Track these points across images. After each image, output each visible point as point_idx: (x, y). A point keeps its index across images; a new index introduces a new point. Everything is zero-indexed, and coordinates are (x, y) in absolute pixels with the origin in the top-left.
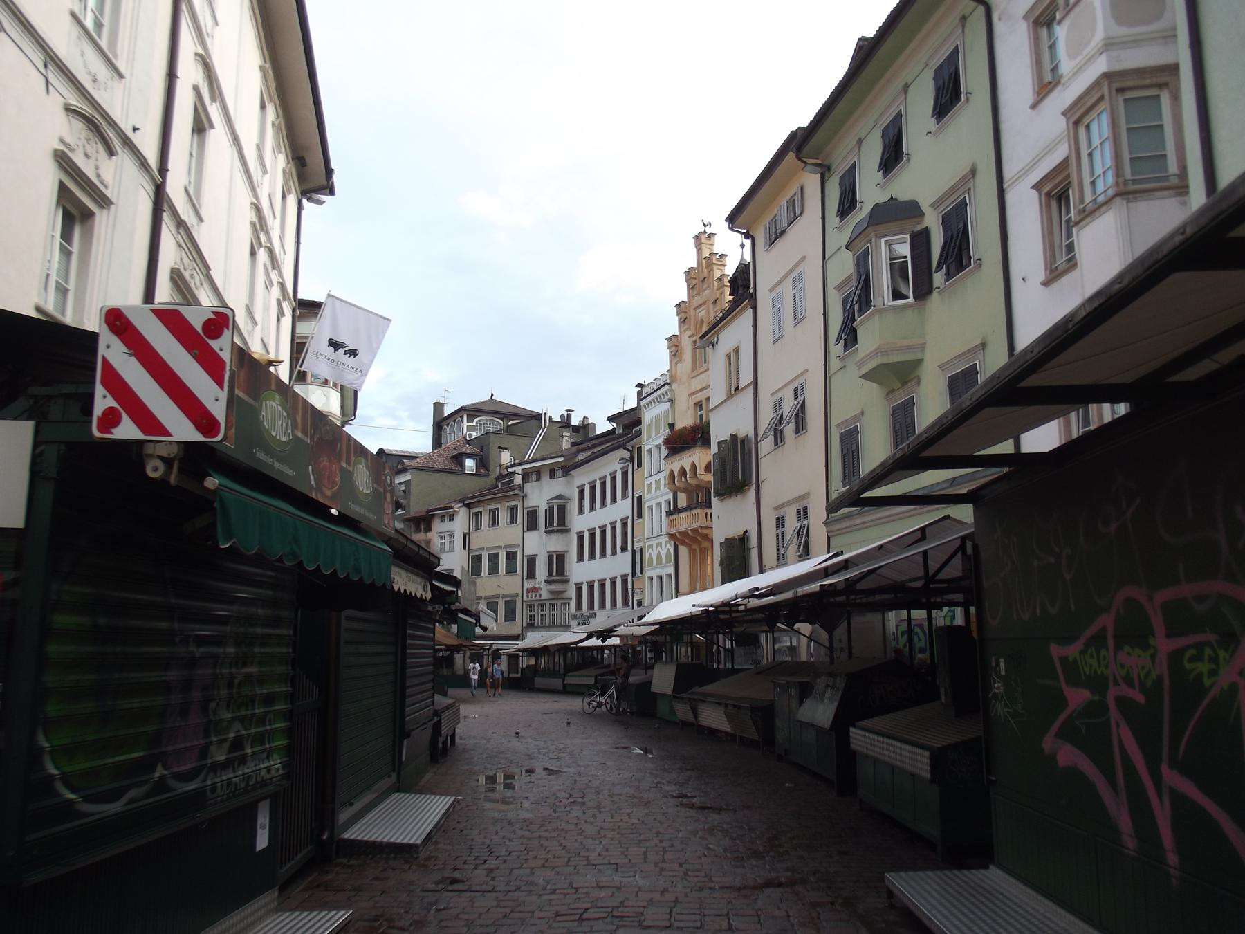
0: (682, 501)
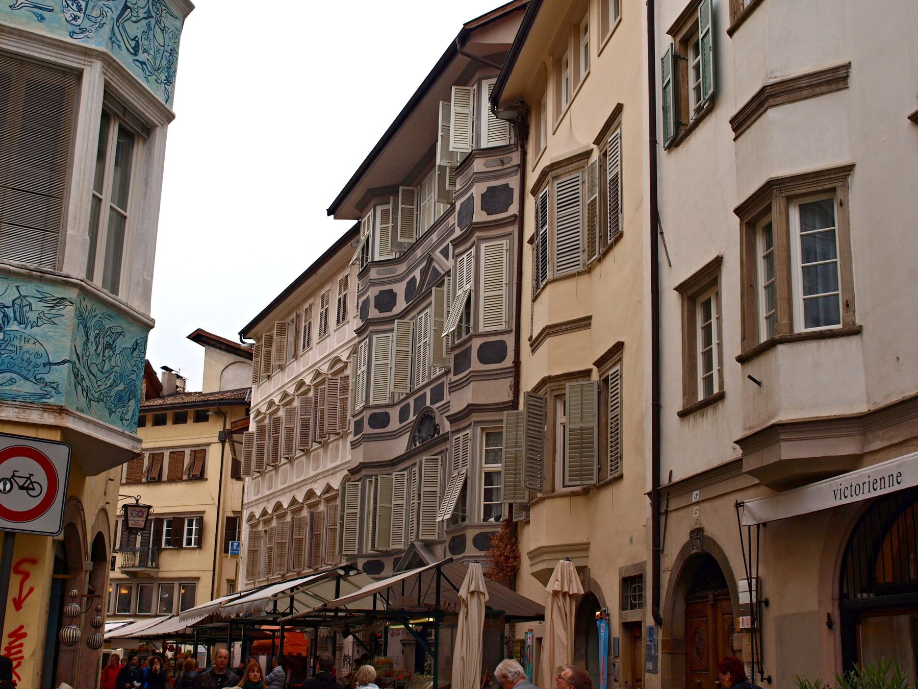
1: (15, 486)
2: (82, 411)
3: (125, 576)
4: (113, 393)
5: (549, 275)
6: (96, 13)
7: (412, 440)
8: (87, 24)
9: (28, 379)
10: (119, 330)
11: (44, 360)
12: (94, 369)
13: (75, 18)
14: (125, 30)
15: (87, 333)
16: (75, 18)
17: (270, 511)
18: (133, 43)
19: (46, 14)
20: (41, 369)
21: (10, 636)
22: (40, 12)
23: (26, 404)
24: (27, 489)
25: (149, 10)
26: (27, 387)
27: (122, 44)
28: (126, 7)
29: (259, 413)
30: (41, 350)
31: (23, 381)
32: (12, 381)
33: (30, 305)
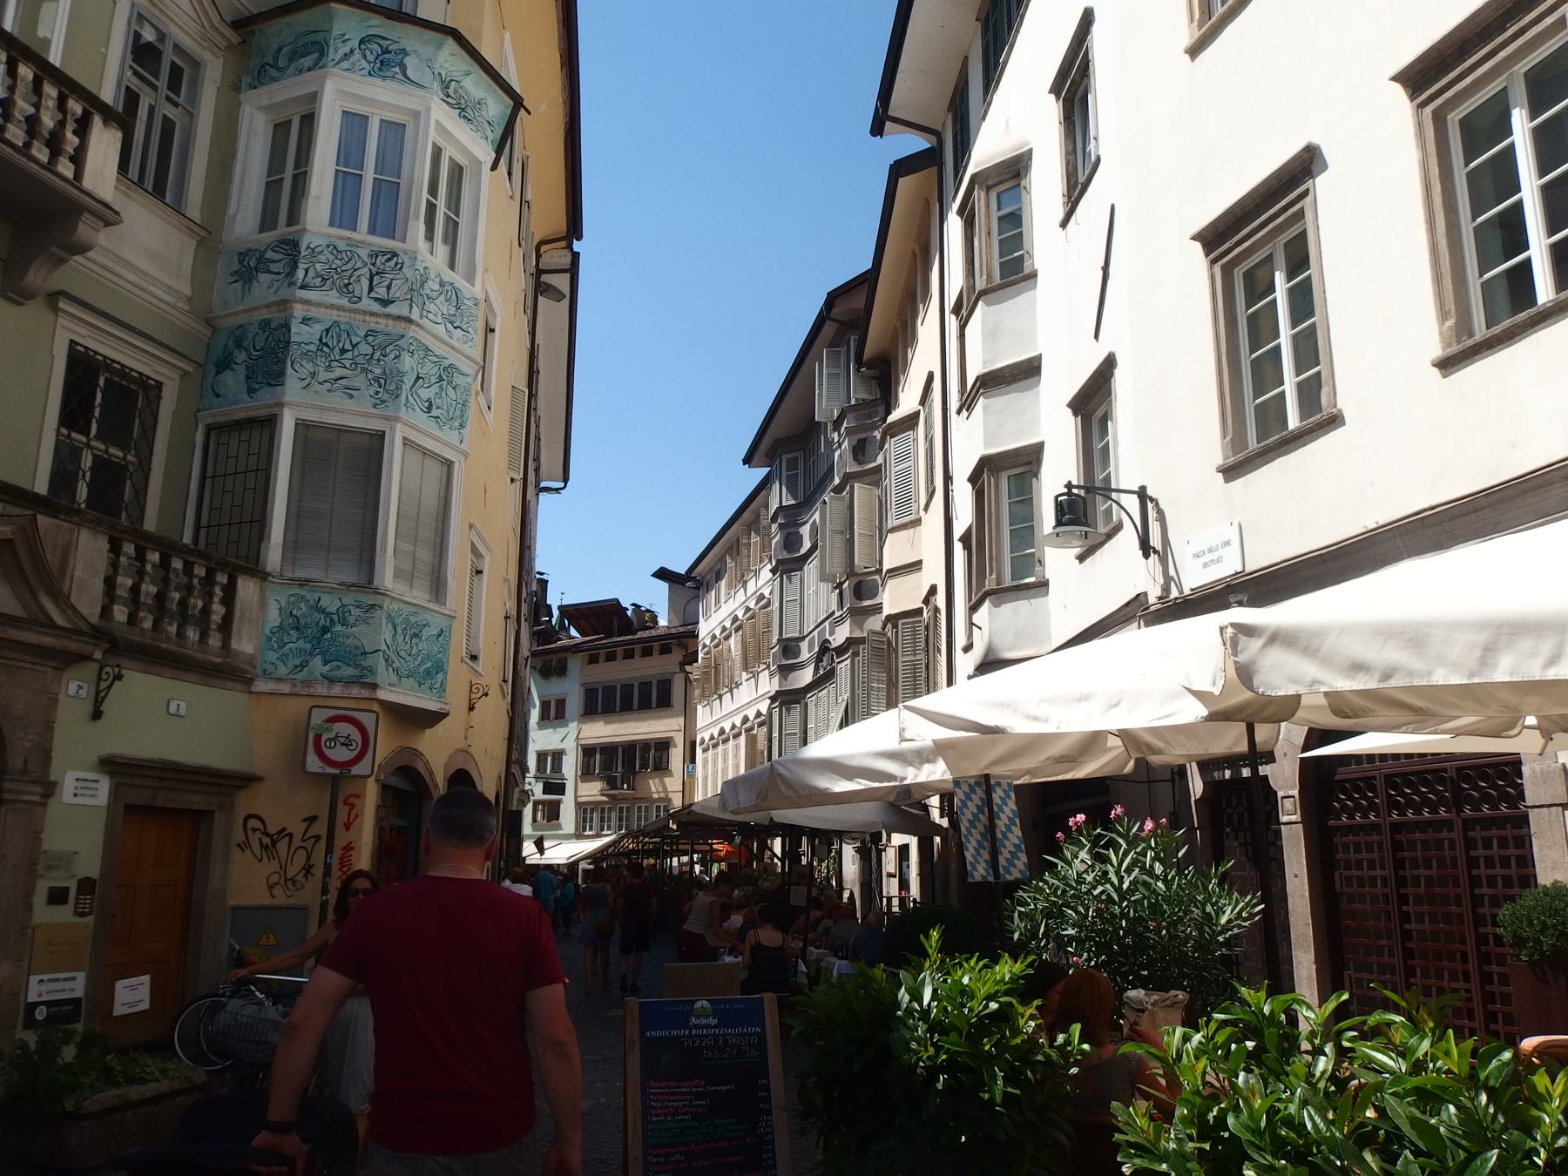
1: (338, 744)
2: (393, 685)
3: (605, 799)
4: (422, 669)
5: (891, 523)
6: (393, 387)
7: (816, 669)
8: (386, 396)
9: (349, 665)
10: (424, 622)
11: (361, 651)
12: (403, 654)
13: (377, 393)
14: (419, 396)
15: (395, 629)
16: (377, 393)
17: (716, 736)
18: (427, 404)
19: (353, 392)
20: (359, 657)
21: (343, 849)
22: (350, 391)
23: (349, 682)
24: (347, 745)
25: (440, 375)
26: (349, 671)
27: (416, 407)
28: (418, 378)
29: (705, 646)
30: (359, 644)
31: (346, 667)
32: (338, 668)
33: (350, 611)
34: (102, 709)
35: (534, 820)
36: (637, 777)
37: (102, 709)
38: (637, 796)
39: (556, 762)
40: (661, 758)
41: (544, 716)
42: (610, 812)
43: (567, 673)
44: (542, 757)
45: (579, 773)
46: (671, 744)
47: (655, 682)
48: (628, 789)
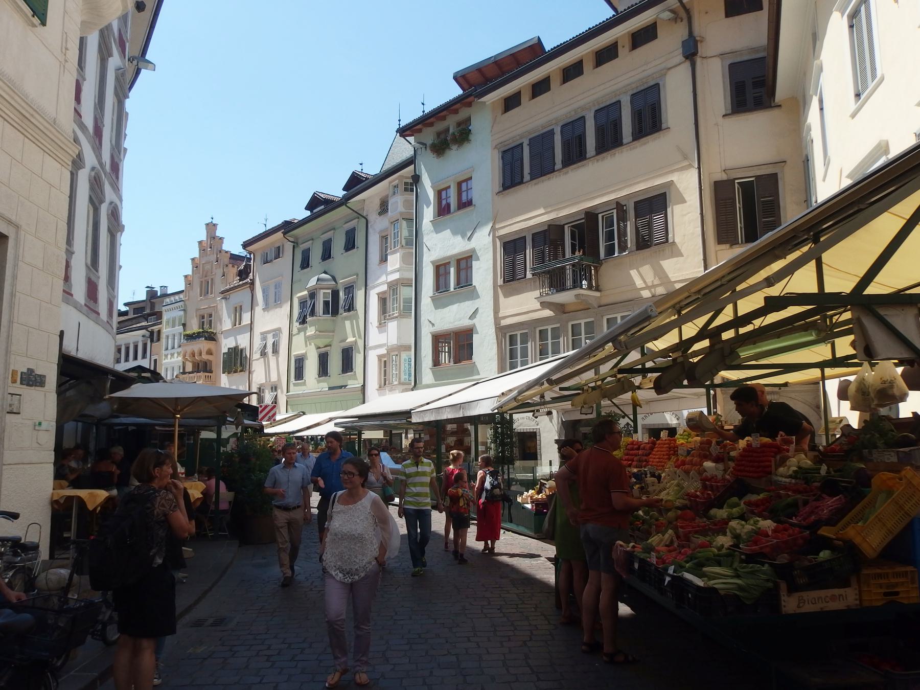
0: (189, 368)
3: (548, 313)
34: (456, 91)
35: (436, 362)
36: (604, 269)
37: (456, 91)
38: (605, 301)
39: (463, 274)
40: (649, 225)
41: (443, 210)
42: (524, 341)
43: (471, 137)
44: (442, 270)
45: (500, 281)
46: (671, 197)
47: (558, 131)
48: (590, 287)
